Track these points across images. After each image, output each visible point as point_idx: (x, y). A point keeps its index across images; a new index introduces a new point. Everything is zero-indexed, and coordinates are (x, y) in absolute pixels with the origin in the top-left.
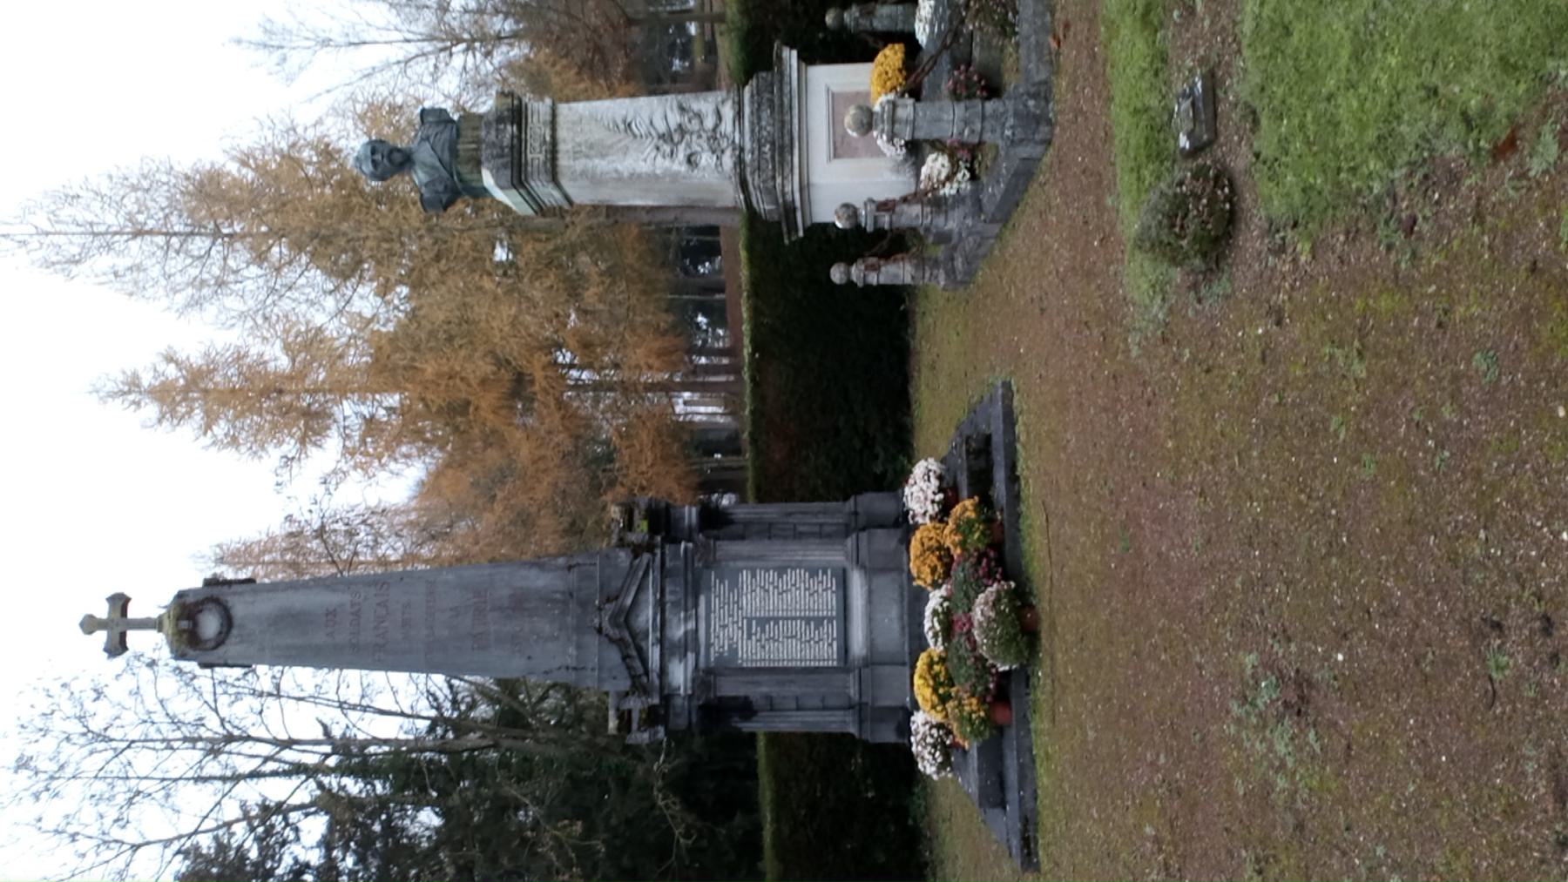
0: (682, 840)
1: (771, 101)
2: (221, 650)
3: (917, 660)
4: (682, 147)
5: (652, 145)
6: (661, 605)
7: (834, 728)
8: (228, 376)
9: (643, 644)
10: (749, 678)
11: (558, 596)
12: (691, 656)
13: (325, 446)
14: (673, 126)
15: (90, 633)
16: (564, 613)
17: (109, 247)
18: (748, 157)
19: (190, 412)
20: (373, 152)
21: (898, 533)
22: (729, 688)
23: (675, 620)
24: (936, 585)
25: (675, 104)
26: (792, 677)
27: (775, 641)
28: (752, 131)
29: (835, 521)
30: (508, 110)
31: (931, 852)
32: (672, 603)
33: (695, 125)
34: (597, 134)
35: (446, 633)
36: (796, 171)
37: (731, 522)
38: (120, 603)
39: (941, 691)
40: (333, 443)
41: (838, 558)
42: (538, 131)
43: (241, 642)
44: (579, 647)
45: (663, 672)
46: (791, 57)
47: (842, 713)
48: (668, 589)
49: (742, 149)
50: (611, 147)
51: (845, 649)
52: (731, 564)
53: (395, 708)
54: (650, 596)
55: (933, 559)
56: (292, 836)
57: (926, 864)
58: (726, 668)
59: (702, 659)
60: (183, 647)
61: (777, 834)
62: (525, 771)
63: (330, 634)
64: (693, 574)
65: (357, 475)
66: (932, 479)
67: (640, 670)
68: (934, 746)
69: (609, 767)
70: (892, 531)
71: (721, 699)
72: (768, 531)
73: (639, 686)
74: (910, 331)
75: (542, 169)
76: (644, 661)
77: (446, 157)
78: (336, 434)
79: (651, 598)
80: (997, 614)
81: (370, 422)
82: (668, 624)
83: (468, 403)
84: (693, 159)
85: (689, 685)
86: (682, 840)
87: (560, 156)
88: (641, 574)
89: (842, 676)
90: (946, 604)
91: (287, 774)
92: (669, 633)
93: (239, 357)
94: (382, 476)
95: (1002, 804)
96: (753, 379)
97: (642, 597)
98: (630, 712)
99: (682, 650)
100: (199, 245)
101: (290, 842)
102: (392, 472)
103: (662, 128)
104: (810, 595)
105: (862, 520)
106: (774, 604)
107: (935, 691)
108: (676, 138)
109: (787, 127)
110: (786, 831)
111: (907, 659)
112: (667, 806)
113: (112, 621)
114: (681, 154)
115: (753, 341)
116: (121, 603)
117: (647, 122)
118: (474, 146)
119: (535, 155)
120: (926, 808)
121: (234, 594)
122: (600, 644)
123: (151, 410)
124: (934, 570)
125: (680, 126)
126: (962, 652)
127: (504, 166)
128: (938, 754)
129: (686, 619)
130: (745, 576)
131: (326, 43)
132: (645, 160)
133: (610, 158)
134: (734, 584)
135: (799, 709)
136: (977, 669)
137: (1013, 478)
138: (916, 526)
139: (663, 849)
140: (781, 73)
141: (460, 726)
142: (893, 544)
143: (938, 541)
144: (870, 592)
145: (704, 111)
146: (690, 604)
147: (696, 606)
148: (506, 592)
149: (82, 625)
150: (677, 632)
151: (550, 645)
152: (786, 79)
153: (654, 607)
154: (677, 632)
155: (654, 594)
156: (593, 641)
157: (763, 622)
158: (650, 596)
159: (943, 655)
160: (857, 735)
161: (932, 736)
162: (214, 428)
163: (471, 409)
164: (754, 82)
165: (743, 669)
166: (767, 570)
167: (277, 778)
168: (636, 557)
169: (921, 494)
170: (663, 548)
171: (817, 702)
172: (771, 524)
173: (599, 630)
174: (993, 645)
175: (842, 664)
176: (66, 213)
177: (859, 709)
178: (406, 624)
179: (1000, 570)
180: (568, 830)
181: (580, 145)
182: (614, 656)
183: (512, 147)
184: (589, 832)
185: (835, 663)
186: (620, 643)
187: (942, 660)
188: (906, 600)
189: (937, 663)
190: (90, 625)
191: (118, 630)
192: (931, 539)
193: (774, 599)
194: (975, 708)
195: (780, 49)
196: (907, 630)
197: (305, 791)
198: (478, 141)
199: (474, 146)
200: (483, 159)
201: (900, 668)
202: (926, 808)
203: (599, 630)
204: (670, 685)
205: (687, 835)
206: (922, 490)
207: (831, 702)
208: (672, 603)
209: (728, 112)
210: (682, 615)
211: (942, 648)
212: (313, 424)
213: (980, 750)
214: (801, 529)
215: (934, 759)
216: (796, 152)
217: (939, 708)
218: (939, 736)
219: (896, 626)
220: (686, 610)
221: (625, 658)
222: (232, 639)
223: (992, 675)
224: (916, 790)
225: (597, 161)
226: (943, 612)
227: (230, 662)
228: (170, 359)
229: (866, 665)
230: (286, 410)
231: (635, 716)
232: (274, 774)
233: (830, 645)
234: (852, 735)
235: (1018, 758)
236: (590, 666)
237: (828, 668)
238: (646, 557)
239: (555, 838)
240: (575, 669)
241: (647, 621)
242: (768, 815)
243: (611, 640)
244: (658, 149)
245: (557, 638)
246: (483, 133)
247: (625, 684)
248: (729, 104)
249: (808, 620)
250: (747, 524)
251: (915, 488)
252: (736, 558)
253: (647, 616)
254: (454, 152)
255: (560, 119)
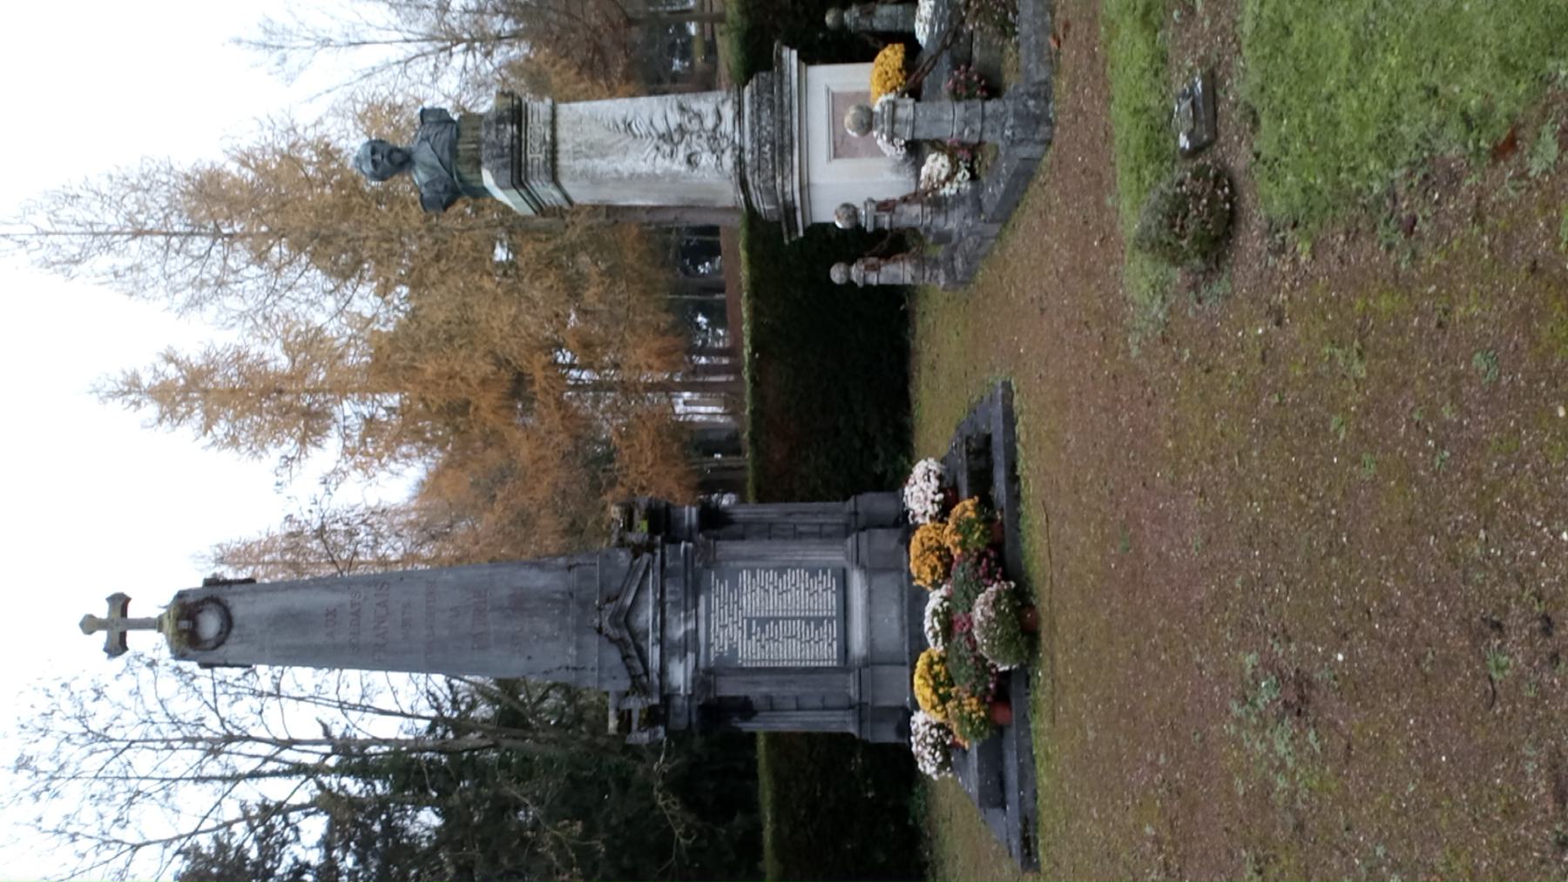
0: (682, 840)
1: (771, 101)
2: (221, 650)
3: (917, 660)
4: (682, 147)
5: (652, 145)
6: (661, 605)
7: (834, 728)
8: (228, 376)
9: (643, 644)
10: (749, 678)
11: (558, 596)
12: (691, 656)
13: (325, 446)
14: (673, 126)
15: (90, 633)
16: (564, 613)
17: (109, 247)
18: (748, 157)
19: (190, 412)
20: (373, 152)
21: (898, 533)
22: (729, 688)
23: (675, 620)
24: (936, 585)
25: (675, 104)
26: (792, 677)
27: (775, 641)
28: (752, 131)
29: (835, 521)
30: (508, 110)
31: (931, 852)
32: (672, 603)
33: (695, 125)
34: (597, 134)
35: (446, 633)
36: (796, 171)
37: (731, 522)
38: (120, 603)
39: (941, 691)
40: (333, 443)
41: (838, 558)
42: (538, 131)
43: (241, 642)
44: (579, 647)
45: (663, 672)
46: (791, 57)
47: (842, 713)
48: (668, 589)
49: (742, 149)
50: (611, 147)
51: (845, 649)
52: (731, 564)
53: (395, 708)
54: (650, 596)
55: (933, 559)
56: (292, 836)
57: (926, 864)
58: (726, 668)
59: (702, 659)
60: (183, 647)
61: (777, 834)
62: (525, 771)
63: (330, 634)
64: (693, 574)
65: (357, 475)
66: (932, 479)
67: (640, 670)
68: (934, 746)
69: (609, 767)
70: (892, 531)
71: (721, 699)
72: (768, 531)
73: (639, 686)
74: (910, 331)
75: (542, 169)
76: (644, 661)
77: (446, 157)
78: (336, 434)
79: (651, 598)
80: (997, 614)
81: (370, 422)
82: (668, 624)
83: (468, 403)
84: (693, 159)
85: (689, 685)
86: (682, 840)
87: (560, 156)
88: (641, 574)
89: (842, 676)
90: (946, 604)
91: (287, 774)
92: (669, 633)
93: (239, 357)
94: (382, 476)
95: (1002, 804)
96: (753, 379)
97: (642, 597)
98: (630, 712)
99: (682, 650)
100: (199, 245)
101: (290, 842)
102: (392, 472)
103: (662, 128)
104: (810, 595)
105: (862, 520)
106: (774, 604)
107: (935, 691)
108: (676, 138)
109: (787, 127)
110: (786, 831)
111: (907, 659)
112: (667, 806)
113: (112, 621)
114: (681, 154)
115: (753, 341)
116: (121, 603)
117: (647, 122)
118: (474, 146)
119: (535, 155)
120: (926, 808)
121: (234, 594)
122: (600, 644)
123: (151, 410)
124: (934, 570)
125: (680, 126)
126: (962, 652)
127: (504, 166)
128: (938, 754)
129: (686, 619)
130: (745, 576)
131: (326, 43)
132: (645, 160)
133: (610, 158)
134: (734, 584)
135: (799, 709)
136: (977, 669)
137: (1013, 478)
138: (916, 526)
139: (663, 849)
140: (781, 73)
141: (460, 726)
142: (893, 544)
143: (938, 541)
144: (870, 592)
145: (704, 111)
146: (690, 604)
147: (696, 606)
148: (506, 592)
149: (82, 625)
150: (677, 632)
151: (550, 645)
152: (786, 79)
153: (654, 607)
154: (677, 632)
155: (654, 594)
156: (593, 641)
157: (763, 622)
158: (650, 596)
159: (943, 655)
160: (857, 735)
161: (932, 736)
162: (214, 428)
163: (471, 409)
164: (754, 82)
165: (743, 669)
166: (767, 570)
167: (277, 778)
168: (636, 557)
169: (921, 494)
170: (663, 548)
171: (817, 702)
172: (771, 524)
173: (599, 630)
174: (993, 645)
175: (842, 664)
176: (66, 213)
177: (859, 709)
178: (406, 624)
179: (1000, 570)
180: (568, 830)
181: (580, 145)
182: (614, 656)
183: (512, 147)
184: (589, 832)
185: (835, 663)
186: (620, 643)
187: (942, 660)
188: (906, 600)
189: (937, 663)
190: (90, 625)
191: (118, 630)
192: (931, 539)
193: (774, 599)
194: (975, 708)
195: (780, 49)
196: (907, 630)
197: (305, 791)
198: (478, 141)
199: (474, 146)
200: (483, 159)
201: (900, 668)
202: (926, 808)
203: (599, 630)
204: (670, 685)
205: (687, 835)
206: (922, 490)
207: (831, 702)
208: (672, 603)
209: (728, 112)
210: (682, 615)
211: (942, 648)
212: (313, 424)
213: (980, 750)
214: (801, 529)
215: (934, 759)
216: (796, 152)
217: (939, 708)
218: (939, 736)
219: (896, 626)
220: (686, 610)
221: (625, 658)
222: (232, 639)
223: (992, 675)
224: (916, 790)
225: (597, 161)
226: (943, 612)
227: (230, 662)
228: (170, 359)
229: (866, 665)
230: (286, 410)
231: (635, 716)
232: (274, 774)
233: (830, 645)
234: (852, 735)
235: (1018, 758)
236: (590, 666)
237: (828, 668)
238: (646, 557)
239: (555, 838)
240: (575, 669)
241: (647, 621)
242: (768, 815)
243: (611, 640)
244: (658, 149)
245: (557, 638)
246: (483, 133)
247: (625, 684)
248: (729, 104)
249: (808, 620)
250: (747, 524)
251: (915, 488)
252: (736, 558)
253: (647, 616)
254: (454, 152)
255: (560, 119)
